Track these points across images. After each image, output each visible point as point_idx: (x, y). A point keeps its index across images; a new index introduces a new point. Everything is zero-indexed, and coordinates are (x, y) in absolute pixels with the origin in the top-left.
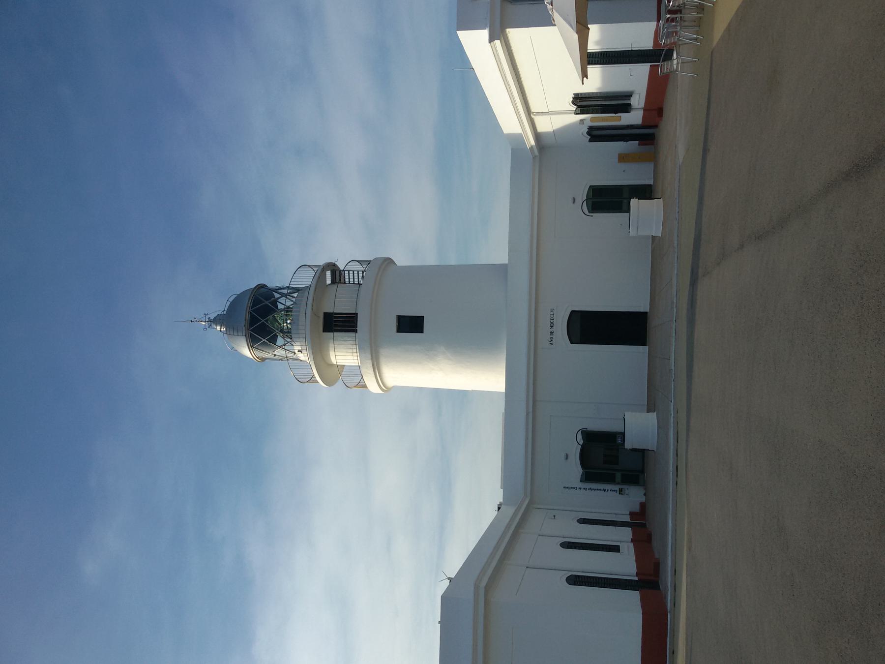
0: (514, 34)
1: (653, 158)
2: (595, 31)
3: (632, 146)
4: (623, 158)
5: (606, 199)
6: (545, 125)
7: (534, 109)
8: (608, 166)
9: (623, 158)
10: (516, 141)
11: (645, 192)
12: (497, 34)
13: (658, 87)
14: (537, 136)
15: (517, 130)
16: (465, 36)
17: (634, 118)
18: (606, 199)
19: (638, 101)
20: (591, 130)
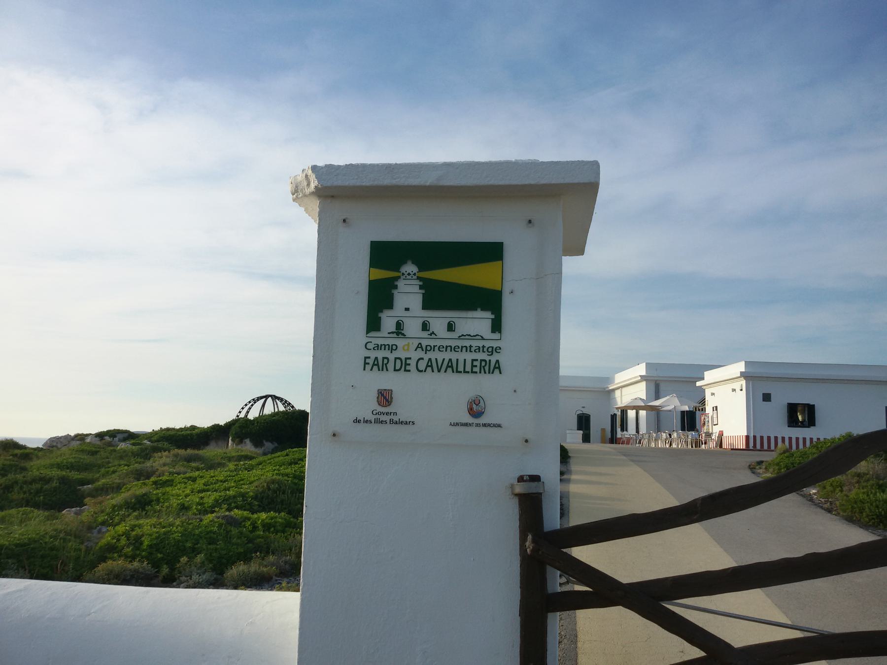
0: (644, 384)
1: (603, 441)
2: (643, 413)
3: (609, 436)
4: (603, 430)
5: (584, 422)
6: (618, 393)
7: (624, 389)
8: (599, 423)
9: (603, 430)
10: (609, 380)
11: (586, 439)
12: (743, 375)
13: (628, 441)
14: (613, 390)
15: (616, 381)
16: (643, 366)
17: (619, 434)
18: (584, 422)
19: (626, 434)
20: (615, 415)
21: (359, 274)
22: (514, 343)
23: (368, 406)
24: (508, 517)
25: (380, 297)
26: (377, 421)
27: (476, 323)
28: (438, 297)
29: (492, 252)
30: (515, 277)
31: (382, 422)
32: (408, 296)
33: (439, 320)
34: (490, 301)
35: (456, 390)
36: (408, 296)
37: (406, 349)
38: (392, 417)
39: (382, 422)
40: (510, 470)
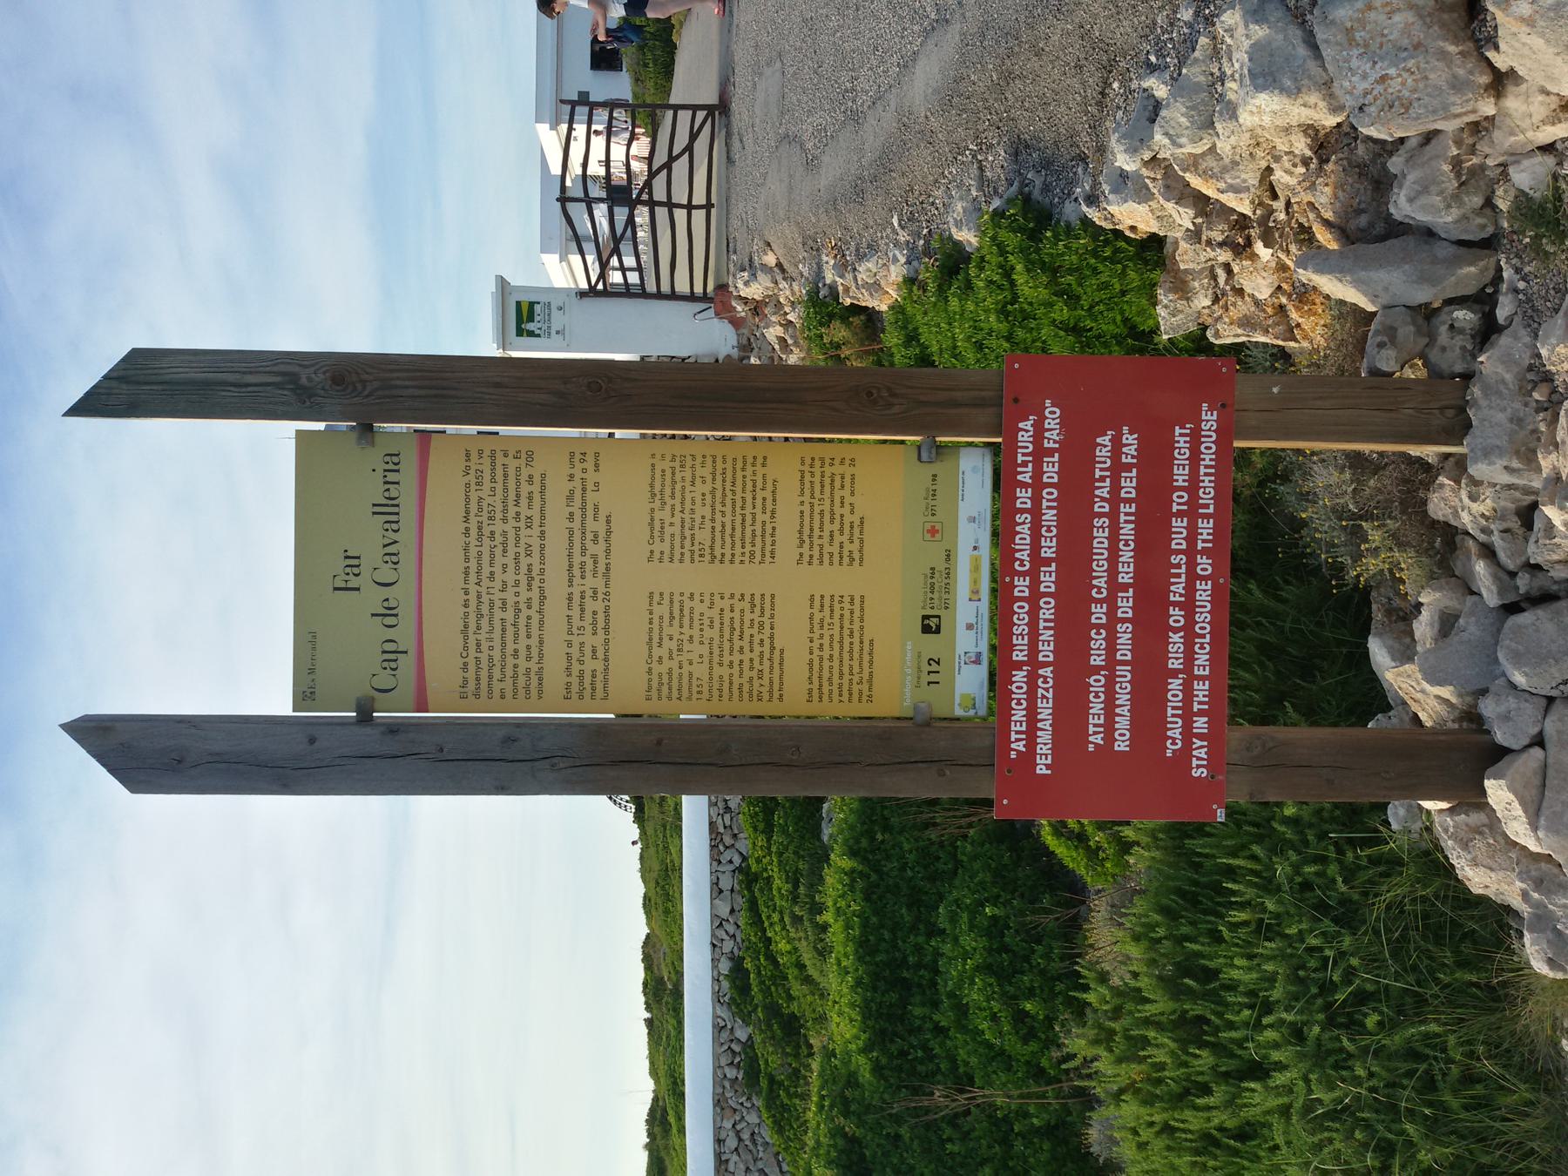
16: (546, 258)
21: (525, 340)
22: (543, 298)
23: (560, 337)
24: (586, 300)
25: (531, 334)
26: (606, 629)
27: (537, 308)
28: (531, 319)
29: (518, 304)
30: (525, 298)
31: (608, 569)
32: (531, 326)
33: (537, 318)
34: (532, 305)
35: (555, 313)
36: (531, 326)
37: (545, 327)
38: (500, 548)
39: (608, 569)
40: (575, 300)
